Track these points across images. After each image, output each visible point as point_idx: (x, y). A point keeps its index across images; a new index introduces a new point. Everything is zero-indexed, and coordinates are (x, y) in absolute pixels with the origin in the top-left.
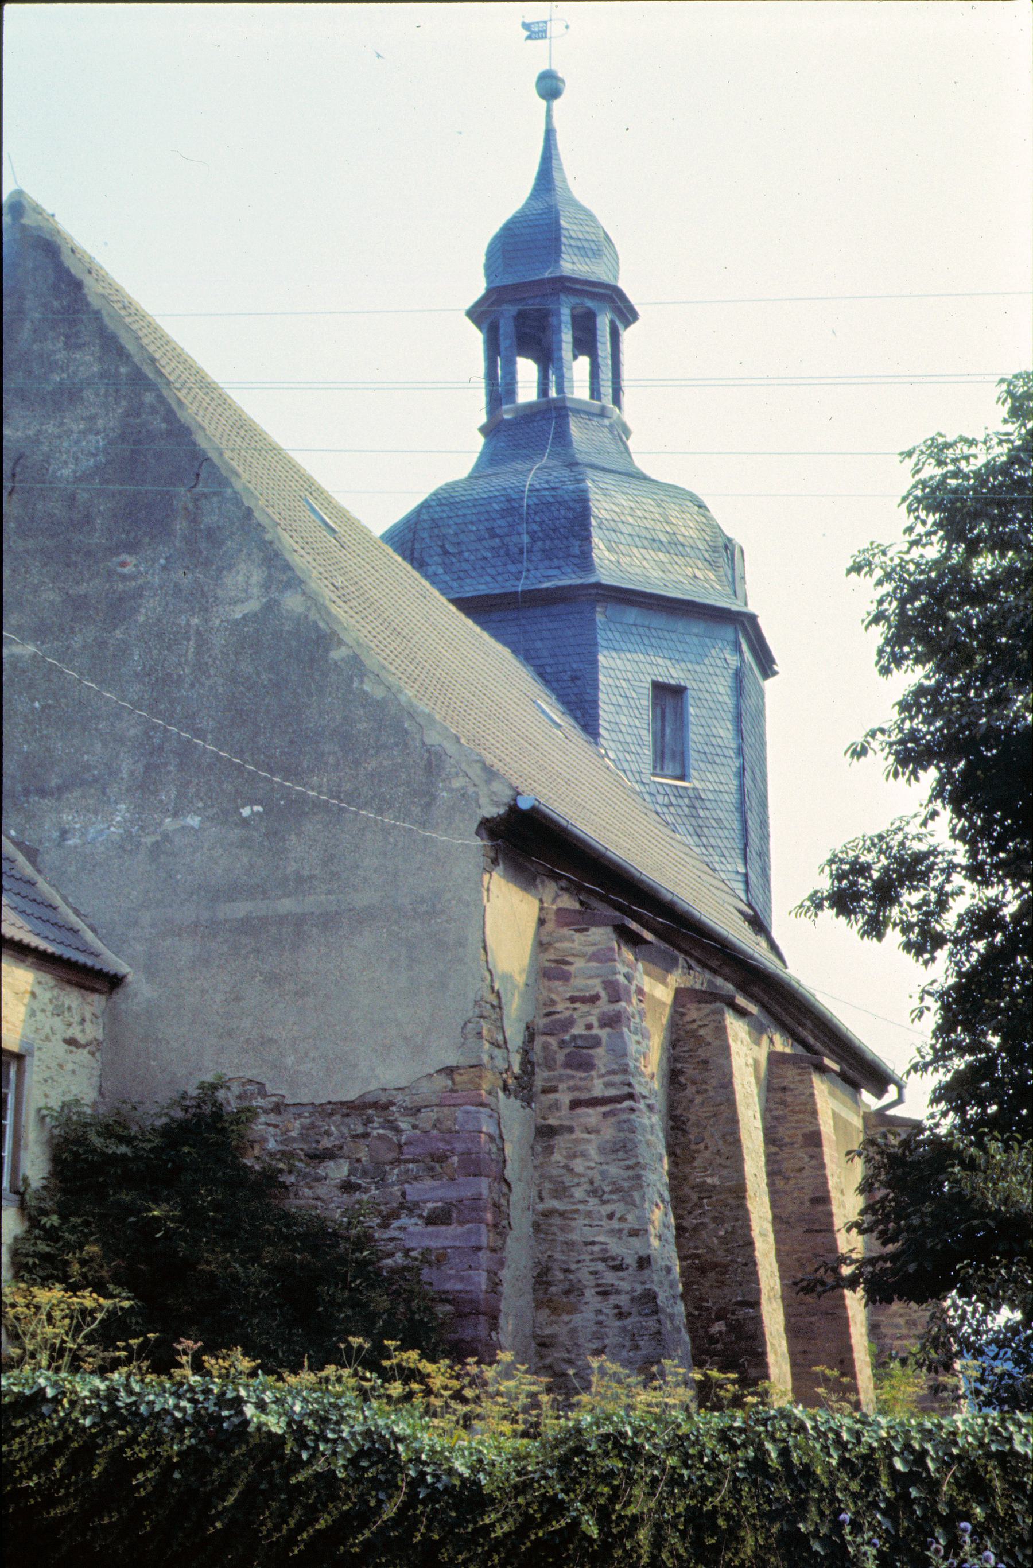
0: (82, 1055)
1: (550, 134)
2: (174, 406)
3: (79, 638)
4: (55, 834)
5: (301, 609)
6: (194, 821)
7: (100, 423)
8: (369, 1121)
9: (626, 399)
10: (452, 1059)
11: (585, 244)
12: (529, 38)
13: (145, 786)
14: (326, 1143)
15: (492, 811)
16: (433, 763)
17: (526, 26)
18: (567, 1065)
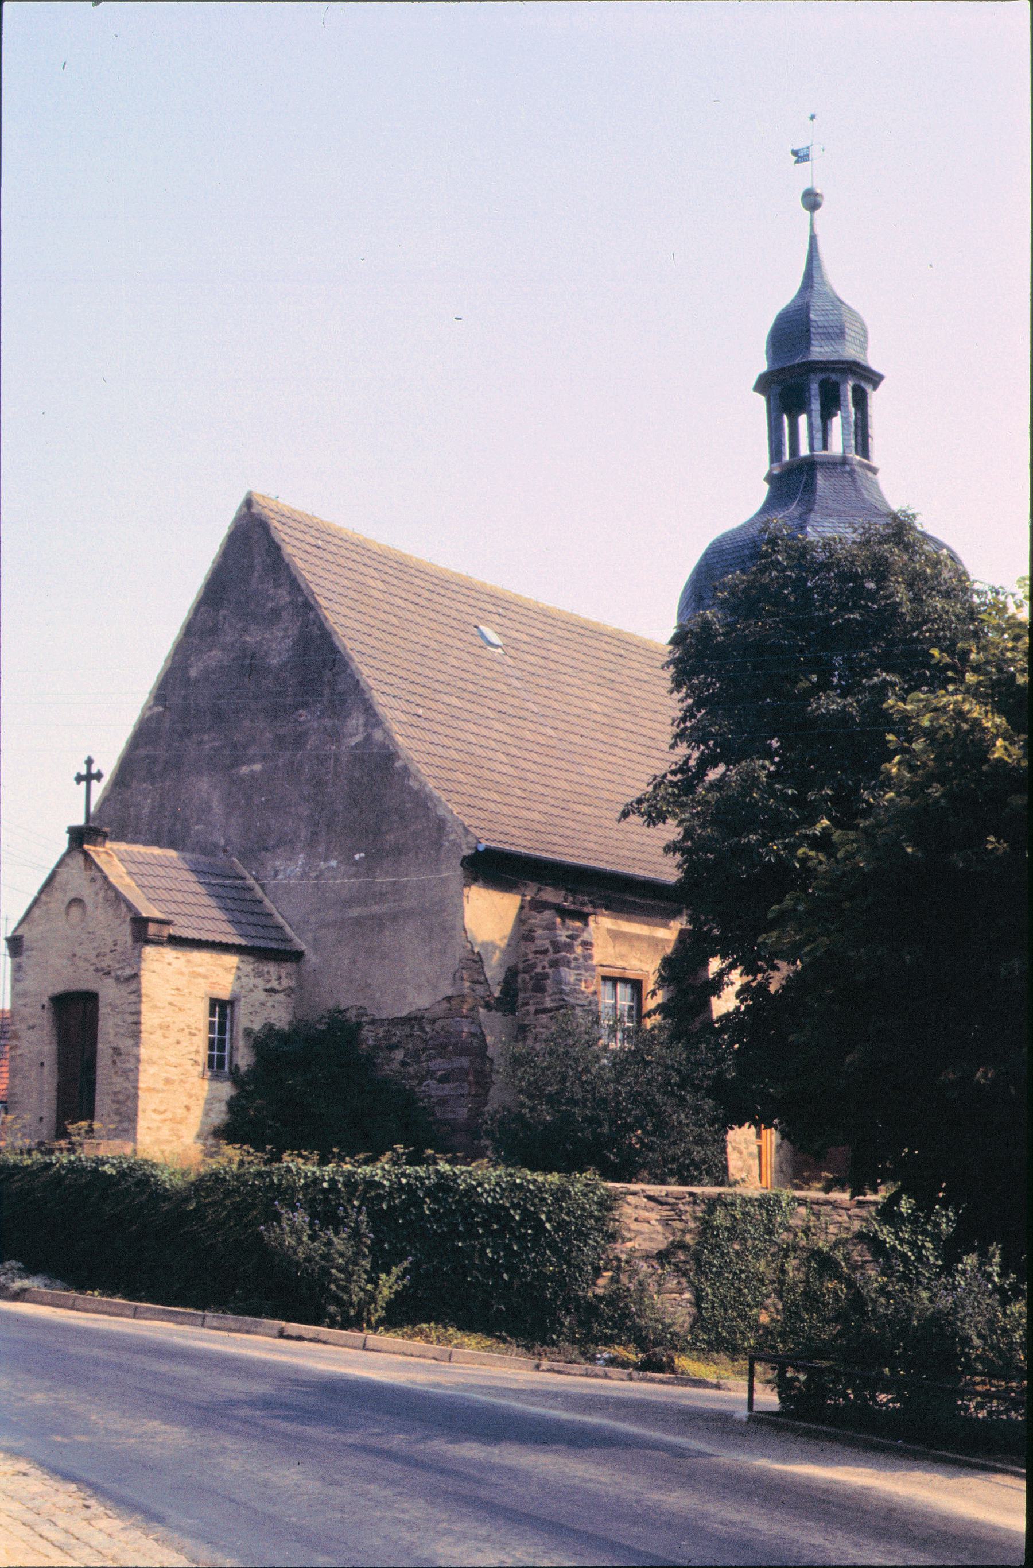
0: (281, 997)
1: (813, 239)
2: (323, 620)
3: (281, 760)
4: (273, 873)
5: (382, 739)
6: (334, 863)
7: (290, 632)
8: (412, 1028)
9: (876, 444)
10: (449, 992)
11: (831, 330)
12: (797, 162)
13: (312, 842)
14: (395, 1040)
15: (467, 852)
16: (441, 825)
17: (795, 153)
18: (533, 990)
